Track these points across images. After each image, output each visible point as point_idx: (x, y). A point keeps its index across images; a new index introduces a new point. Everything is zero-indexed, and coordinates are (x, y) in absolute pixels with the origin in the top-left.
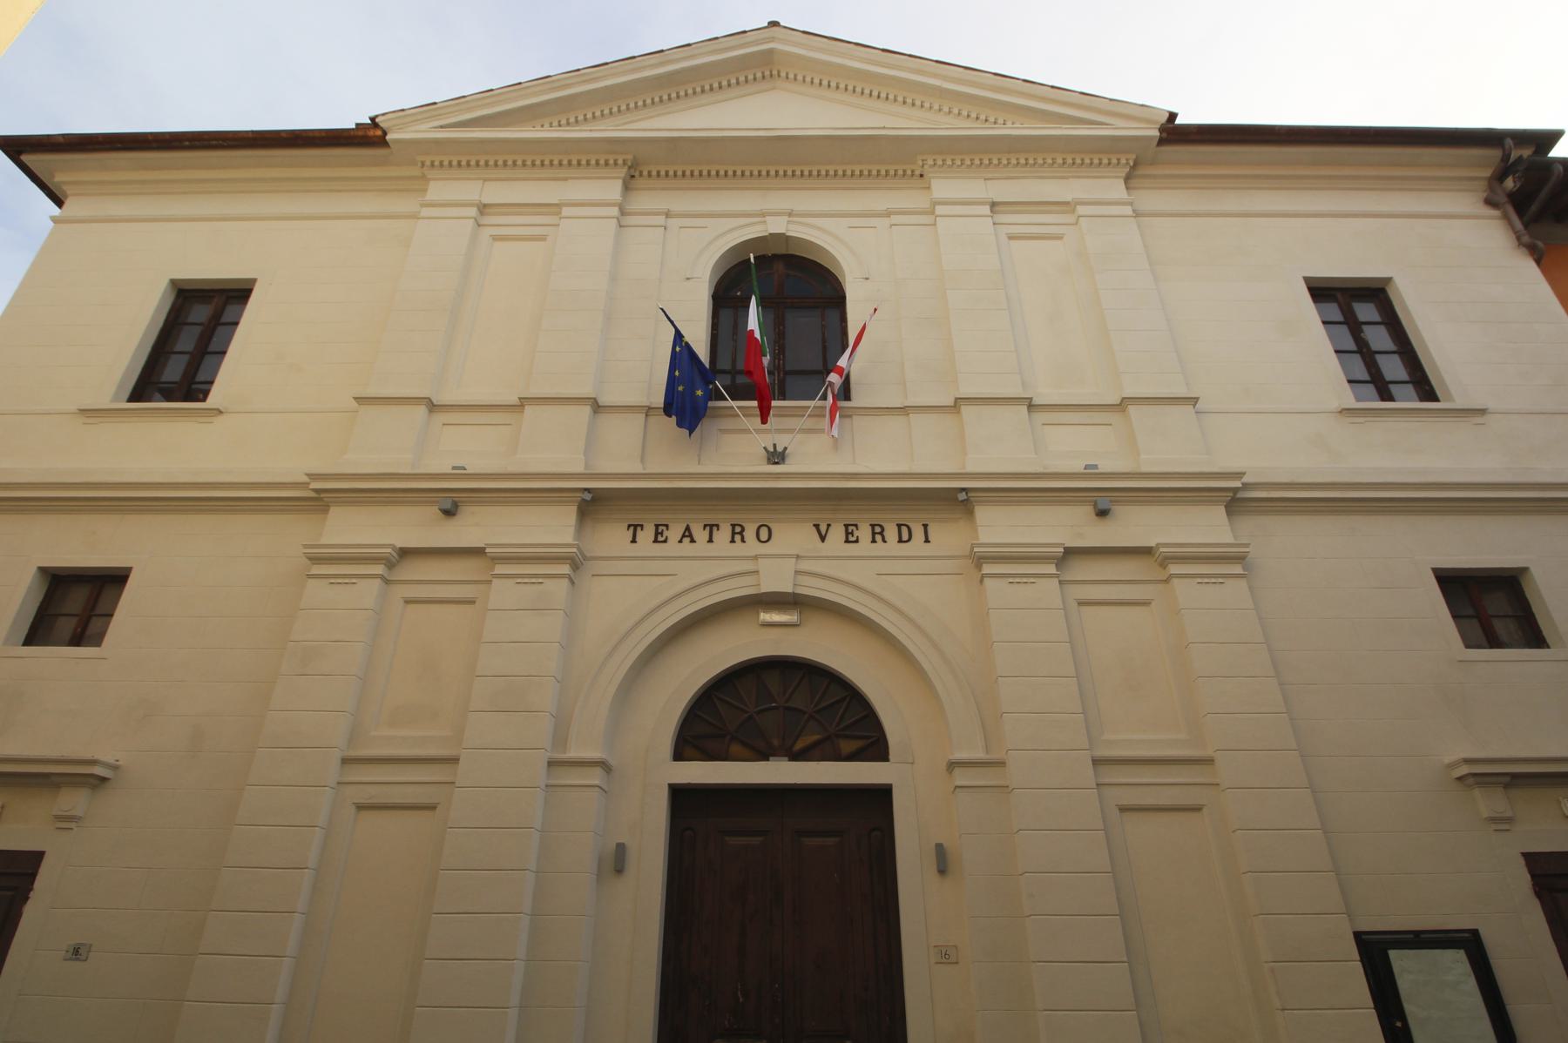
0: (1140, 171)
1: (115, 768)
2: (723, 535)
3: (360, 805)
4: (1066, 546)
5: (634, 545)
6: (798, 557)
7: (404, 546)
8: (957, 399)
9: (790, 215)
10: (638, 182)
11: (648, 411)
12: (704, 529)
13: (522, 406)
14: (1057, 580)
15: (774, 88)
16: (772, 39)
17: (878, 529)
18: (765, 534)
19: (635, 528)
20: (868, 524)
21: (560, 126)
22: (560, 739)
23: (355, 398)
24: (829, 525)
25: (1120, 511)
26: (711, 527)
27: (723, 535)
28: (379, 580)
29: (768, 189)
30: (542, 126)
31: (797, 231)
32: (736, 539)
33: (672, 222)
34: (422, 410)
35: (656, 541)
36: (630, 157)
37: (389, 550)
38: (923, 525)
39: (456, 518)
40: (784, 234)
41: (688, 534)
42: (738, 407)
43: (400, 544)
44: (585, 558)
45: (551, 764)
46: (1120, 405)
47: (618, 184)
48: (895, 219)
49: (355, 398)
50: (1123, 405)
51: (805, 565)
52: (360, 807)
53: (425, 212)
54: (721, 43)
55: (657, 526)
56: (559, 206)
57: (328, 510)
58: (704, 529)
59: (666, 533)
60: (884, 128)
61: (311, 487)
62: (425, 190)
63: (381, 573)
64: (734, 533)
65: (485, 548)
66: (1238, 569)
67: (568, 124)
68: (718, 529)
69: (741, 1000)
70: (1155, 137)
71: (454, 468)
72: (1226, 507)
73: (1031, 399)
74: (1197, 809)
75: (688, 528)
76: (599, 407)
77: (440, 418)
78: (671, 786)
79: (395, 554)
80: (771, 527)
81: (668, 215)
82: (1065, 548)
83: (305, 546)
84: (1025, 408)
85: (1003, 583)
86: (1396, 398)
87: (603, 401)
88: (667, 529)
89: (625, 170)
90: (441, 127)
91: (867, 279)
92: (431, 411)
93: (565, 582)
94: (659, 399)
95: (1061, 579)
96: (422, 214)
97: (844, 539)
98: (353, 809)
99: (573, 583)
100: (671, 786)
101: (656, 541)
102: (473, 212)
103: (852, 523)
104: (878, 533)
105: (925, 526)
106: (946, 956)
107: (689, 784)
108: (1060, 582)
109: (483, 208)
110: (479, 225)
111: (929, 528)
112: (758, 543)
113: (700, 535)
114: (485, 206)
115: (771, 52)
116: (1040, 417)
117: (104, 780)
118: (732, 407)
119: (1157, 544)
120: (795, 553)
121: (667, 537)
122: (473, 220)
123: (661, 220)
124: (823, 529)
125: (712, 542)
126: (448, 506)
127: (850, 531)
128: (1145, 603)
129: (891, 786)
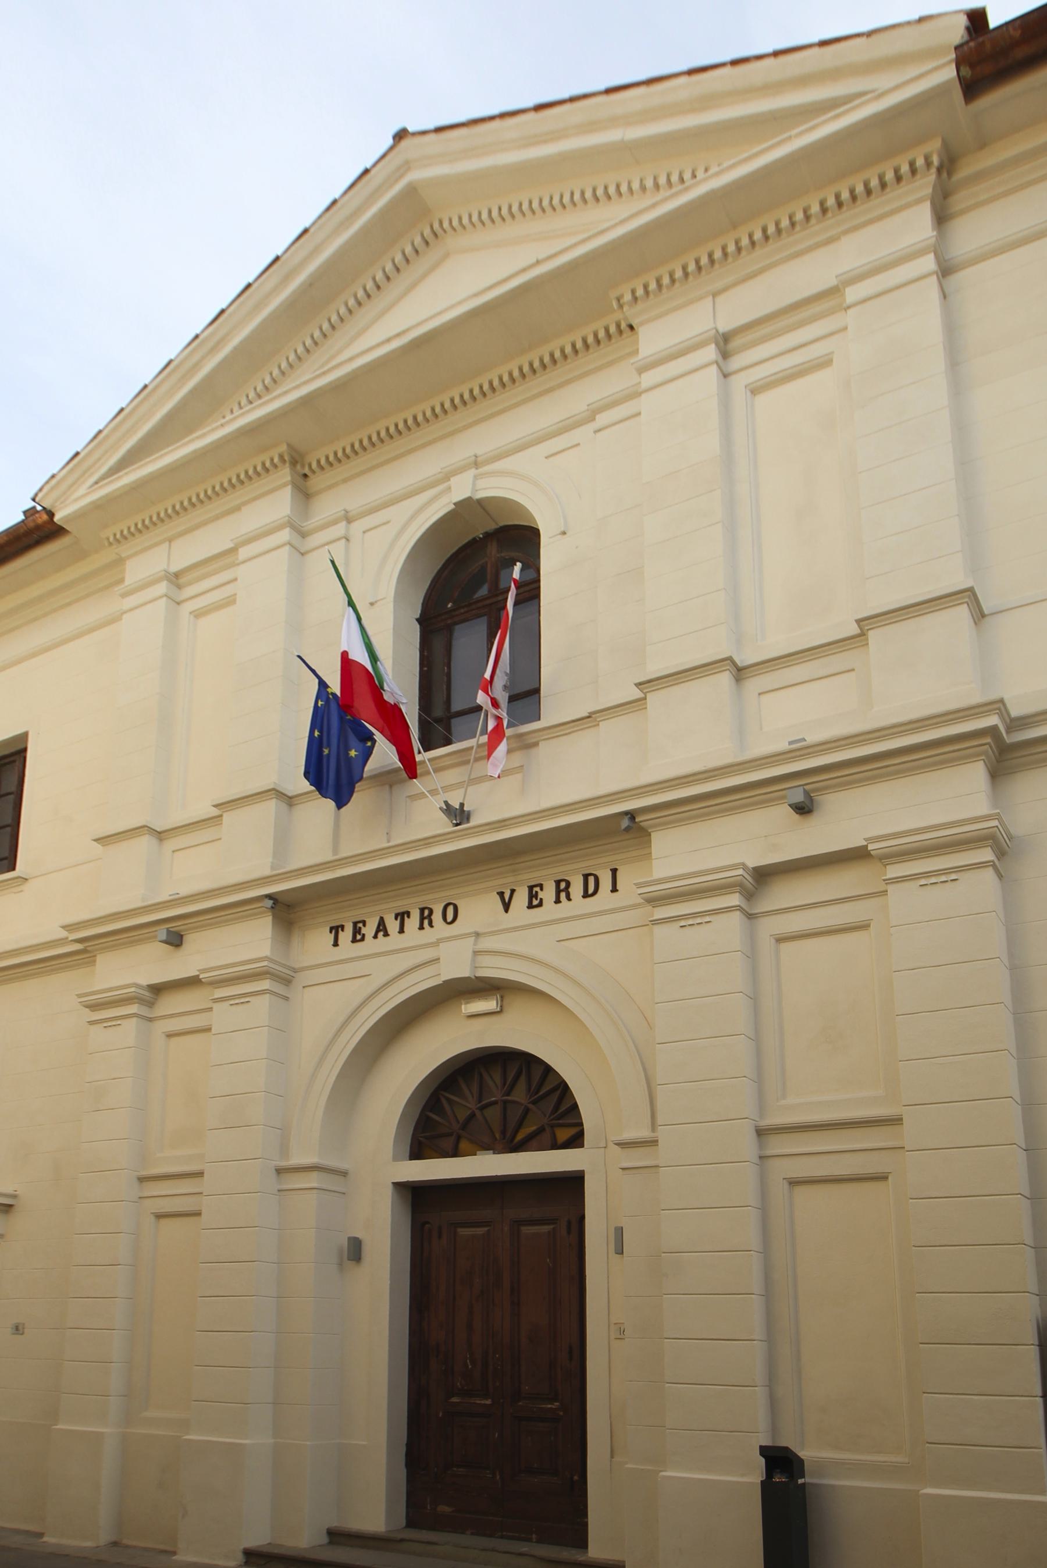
0: (963, 172)
1: (15, 1197)
2: (413, 922)
5: (615, 894)
6: (477, 935)
7: (503, 911)
9: (476, 464)
10: (317, 481)
13: (863, 634)
15: (447, 256)
17: (563, 885)
18: (452, 913)
19: (336, 930)
20: (495, 893)
22: (284, 1149)
23: (214, 806)
24: (513, 891)
25: (192, 941)
26: (402, 916)
28: (738, 913)
29: (452, 433)
31: (490, 488)
32: (561, 899)
33: (358, 526)
34: (271, 807)
35: (530, 906)
37: (740, 872)
39: (815, 814)
40: (469, 499)
43: (752, 864)
44: (295, 971)
47: (286, 495)
48: (602, 419)
49: (214, 806)
51: (486, 944)
53: (649, 378)
55: (531, 888)
56: (233, 551)
57: (95, 961)
58: (331, 932)
59: (541, 895)
60: (538, 262)
61: (70, 939)
62: (637, 351)
63: (737, 903)
64: (558, 892)
65: (867, 846)
69: (470, 1367)
71: (790, 743)
74: (883, 1178)
76: (290, 798)
77: (171, 844)
79: (147, 994)
80: (597, 874)
81: (348, 519)
83: (79, 996)
84: (725, 679)
85: (674, 927)
87: (745, 658)
88: (542, 889)
89: (932, 177)
90: (96, 483)
91: (564, 533)
93: (989, 874)
96: (644, 385)
98: (153, 1218)
99: (1000, 876)
101: (530, 906)
102: (162, 588)
105: (614, 871)
109: (176, 579)
110: (178, 603)
111: (618, 873)
112: (444, 923)
114: (177, 575)
115: (411, 191)
117: (11, 1206)
120: (472, 930)
122: (287, 548)
123: (340, 529)
124: (507, 897)
125: (617, 891)
126: (799, 797)
129: (584, 1171)
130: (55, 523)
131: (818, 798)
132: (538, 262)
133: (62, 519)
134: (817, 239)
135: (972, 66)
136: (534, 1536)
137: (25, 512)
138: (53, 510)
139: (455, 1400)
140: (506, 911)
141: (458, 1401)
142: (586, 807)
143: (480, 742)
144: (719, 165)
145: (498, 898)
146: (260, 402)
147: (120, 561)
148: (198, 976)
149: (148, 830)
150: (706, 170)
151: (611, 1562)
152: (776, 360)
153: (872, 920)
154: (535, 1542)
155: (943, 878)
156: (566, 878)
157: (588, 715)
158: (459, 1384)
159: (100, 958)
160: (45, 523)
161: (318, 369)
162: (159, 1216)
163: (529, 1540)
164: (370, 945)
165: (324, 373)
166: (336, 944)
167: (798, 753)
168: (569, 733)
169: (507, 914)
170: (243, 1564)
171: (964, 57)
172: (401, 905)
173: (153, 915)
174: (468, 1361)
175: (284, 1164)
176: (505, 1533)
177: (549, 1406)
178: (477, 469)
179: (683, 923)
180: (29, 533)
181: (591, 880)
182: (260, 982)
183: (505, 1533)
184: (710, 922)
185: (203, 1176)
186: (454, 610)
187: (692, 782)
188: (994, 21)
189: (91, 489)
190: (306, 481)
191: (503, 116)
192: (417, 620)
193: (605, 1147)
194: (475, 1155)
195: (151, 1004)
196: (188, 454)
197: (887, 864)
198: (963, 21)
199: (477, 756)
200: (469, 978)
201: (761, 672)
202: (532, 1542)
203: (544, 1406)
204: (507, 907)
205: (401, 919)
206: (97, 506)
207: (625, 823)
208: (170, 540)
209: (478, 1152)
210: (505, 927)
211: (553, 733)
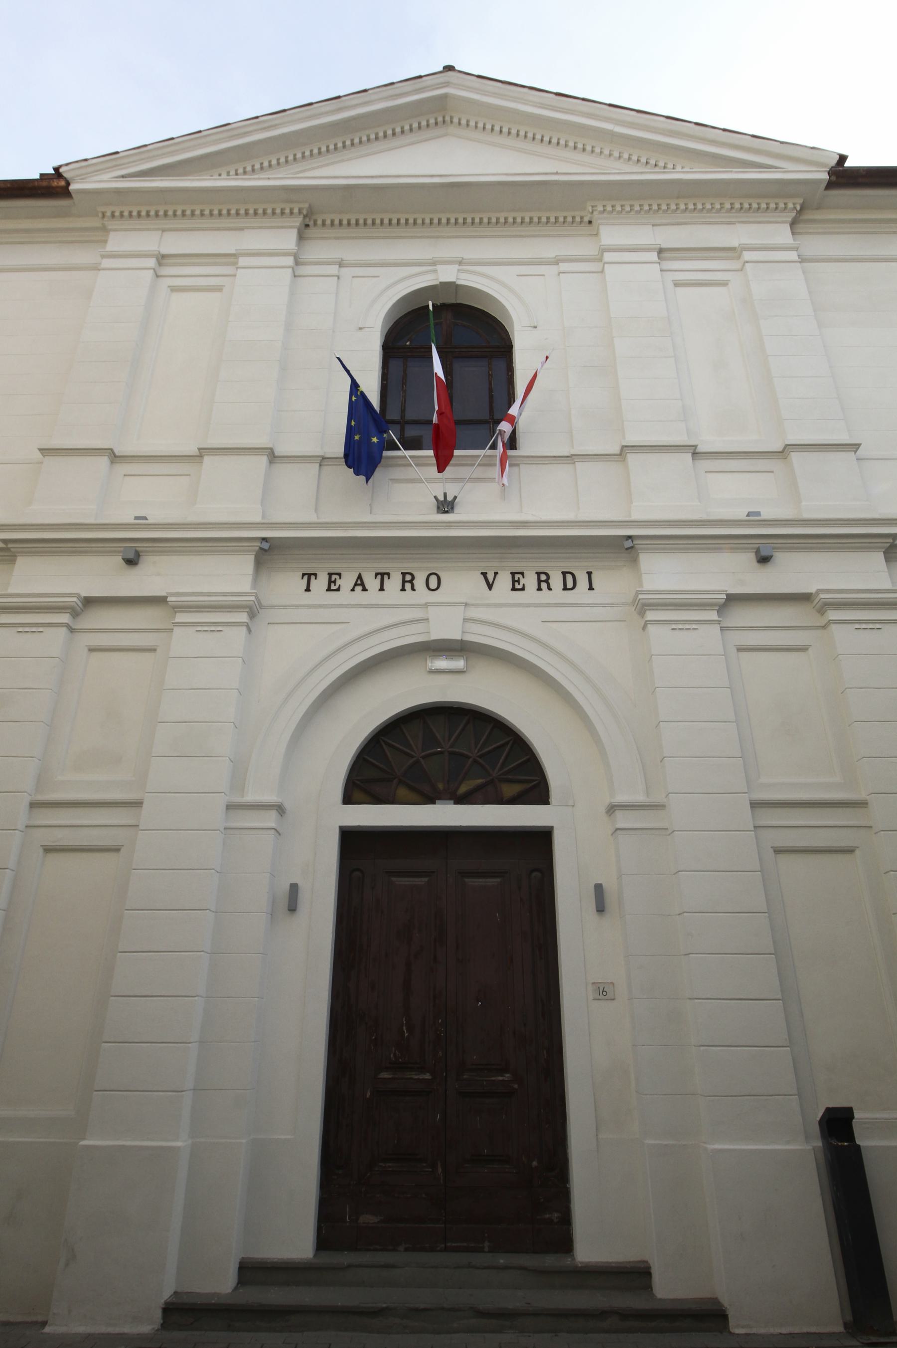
6: (466, 605)
9: (460, 263)
10: (311, 232)
15: (446, 135)
16: (447, 84)
18: (434, 582)
19: (309, 576)
24: (496, 574)
26: (382, 576)
30: (220, 175)
31: (467, 279)
33: (344, 271)
42: (411, 457)
47: (293, 234)
48: (564, 267)
50: (784, 452)
51: (473, 613)
60: (557, 173)
69: (406, 1035)
74: (850, 851)
75: (360, 577)
82: (727, 595)
90: (123, 177)
91: (535, 327)
98: (41, 851)
102: (152, 262)
105: (589, 574)
109: (162, 259)
111: (593, 576)
112: (433, 592)
113: (372, 583)
114: (164, 256)
115: (445, 97)
116: (122, 468)
118: (405, 457)
123: (334, 269)
127: (516, 579)
130: (68, 189)
132: (557, 173)
133: (74, 189)
134: (724, 220)
135: (837, 177)
136: (487, 1244)
137: (41, 175)
138: (70, 181)
139: (385, 1075)
141: (390, 1076)
143: (486, 454)
144: (682, 168)
147: (105, 230)
148: (166, 597)
149: (110, 453)
150: (682, 168)
154: (489, 1252)
157: (570, 455)
159: (20, 560)
160: (62, 187)
162: (48, 850)
163: (481, 1250)
164: (345, 596)
167: (769, 523)
168: (547, 464)
169: (491, 592)
170: (160, 1327)
171: (831, 172)
172: (383, 567)
175: (237, 799)
176: (449, 1244)
177: (501, 1078)
178: (459, 265)
180: (40, 188)
181: (569, 578)
183: (449, 1244)
185: (142, 807)
186: (409, 348)
188: (848, 164)
190: (305, 229)
191: (584, 99)
193: (573, 806)
194: (435, 804)
195: (75, 614)
198: (837, 157)
199: (481, 463)
202: (484, 1252)
203: (493, 1078)
206: (118, 192)
207: (628, 544)
208: (163, 231)
209: (437, 801)
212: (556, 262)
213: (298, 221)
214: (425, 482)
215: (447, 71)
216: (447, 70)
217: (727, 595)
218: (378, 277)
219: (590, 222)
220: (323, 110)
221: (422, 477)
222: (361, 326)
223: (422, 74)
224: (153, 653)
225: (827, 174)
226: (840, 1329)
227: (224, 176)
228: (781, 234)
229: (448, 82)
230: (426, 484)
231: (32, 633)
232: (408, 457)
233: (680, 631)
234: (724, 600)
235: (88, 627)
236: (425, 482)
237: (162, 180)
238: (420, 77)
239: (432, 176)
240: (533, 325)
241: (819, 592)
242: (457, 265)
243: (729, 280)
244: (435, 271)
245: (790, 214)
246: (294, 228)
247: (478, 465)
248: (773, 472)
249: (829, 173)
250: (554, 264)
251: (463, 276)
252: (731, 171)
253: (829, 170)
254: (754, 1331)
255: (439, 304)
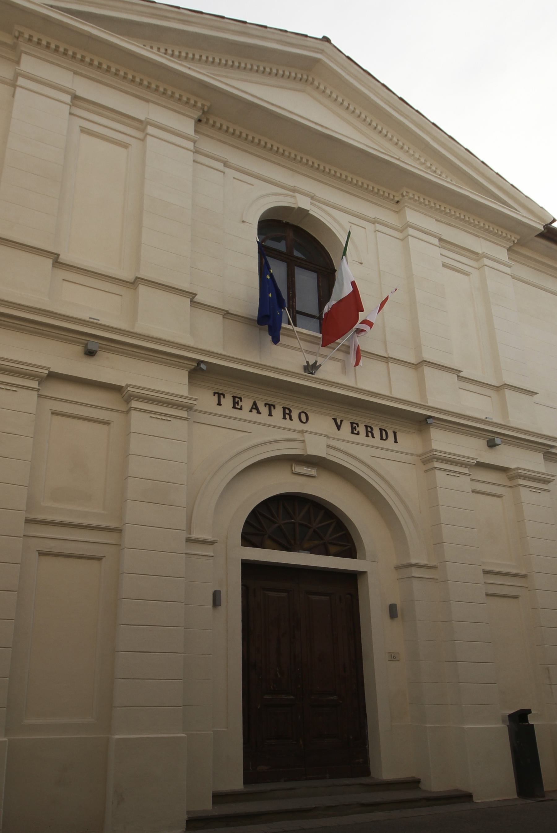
2: (278, 412)
3: (488, 594)
4: (51, 370)
5: (250, 413)
8: (137, 278)
11: (246, 320)
12: (214, 395)
14: (36, 393)
16: (322, 52)
18: (304, 418)
20: (349, 422)
21: (165, 54)
24: (342, 421)
26: (271, 407)
27: (278, 412)
30: (152, 48)
31: (315, 212)
36: (208, 104)
38: (394, 432)
39: (95, 357)
41: (255, 407)
42: (297, 332)
45: (28, 521)
46: (133, 283)
48: (379, 227)
50: (499, 388)
52: (41, 554)
54: (287, 36)
58: (214, 395)
60: (399, 159)
66: (184, 414)
67: (172, 55)
68: (224, 397)
69: (279, 676)
70: (539, 229)
71: (90, 318)
72: (190, 372)
73: (58, 255)
74: (516, 597)
75: (255, 403)
78: (242, 560)
82: (50, 372)
84: (49, 262)
85: (444, 474)
86: (297, 325)
90: (52, 6)
91: (361, 263)
92: (53, 266)
94: (255, 313)
95: (40, 393)
97: (232, 406)
100: (242, 560)
103: (356, 422)
104: (369, 431)
105: (395, 433)
106: (393, 657)
107: (254, 560)
108: (39, 396)
112: (304, 424)
113: (264, 410)
115: (318, 61)
116: (62, 274)
118: (293, 330)
119: (127, 385)
121: (241, 406)
123: (220, 166)
127: (236, 401)
128: (107, 423)
131: (99, 353)
139: (267, 697)
140: (339, 429)
142: (157, 342)
145: (333, 421)
146: (163, 55)
151: (389, 781)
152: (102, 127)
153: (113, 421)
155: (163, 418)
156: (306, 412)
158: (271, 687)
161: (211, 73)
164: (245, 413)
165: (214, 78)
166: (219, 404)
172: (271, 400)
173: (510, 432)
174: (278, 673)
179: (448, 473)
182: (462, 468)
184: (459, 477)
187: (125, 335)
189: (42, 5)
192: (336, 270)
196: (156, 61)
197: (132, 400)
198: (553, 219)
200: (303, 455)
201: (72, 271)
204: (339, 428)
205: (338, 424)
209: (300, 551)
210: (340, 438)
211: (365, 354)
212: (374, 222)
213: (197, 114)
214: (304, 352)
215: (326, 41)
216: (326, 40)
217: (50, 372)
218: (253, 185)
219: (398, 202)
220: (233, 28)
221: (302, 347)
222: (244, 220)
223: (309, 35)
224: (107, 426)
225: (543, 227)
226: (516, 796)
227: (155, 50)
228: (503, 254)
229: (323, 51)
230: (305, 354)
231: (7, 390)
232: (295, 332)
233: (454, 477)
234: (46, 374)
235: (48, 395)
236: (304, 352)
237: (92, 27)
238: (306, 36)
239: (316, 123)
240: (360, 261)
241: (127, 386)
242: (310, 199)
243: (471, 273)
244: (294, 197)
245: (510, 243)
246: (193, 119)
247: (337, 350)
248: (491, 397)
249: (544, 227)
250: (372, 223)
251: (313, 208)
252: (496, 203)
253: (545, 225)
254: (483, 801)
255: (284, 222)
